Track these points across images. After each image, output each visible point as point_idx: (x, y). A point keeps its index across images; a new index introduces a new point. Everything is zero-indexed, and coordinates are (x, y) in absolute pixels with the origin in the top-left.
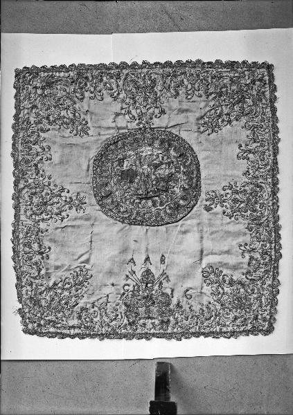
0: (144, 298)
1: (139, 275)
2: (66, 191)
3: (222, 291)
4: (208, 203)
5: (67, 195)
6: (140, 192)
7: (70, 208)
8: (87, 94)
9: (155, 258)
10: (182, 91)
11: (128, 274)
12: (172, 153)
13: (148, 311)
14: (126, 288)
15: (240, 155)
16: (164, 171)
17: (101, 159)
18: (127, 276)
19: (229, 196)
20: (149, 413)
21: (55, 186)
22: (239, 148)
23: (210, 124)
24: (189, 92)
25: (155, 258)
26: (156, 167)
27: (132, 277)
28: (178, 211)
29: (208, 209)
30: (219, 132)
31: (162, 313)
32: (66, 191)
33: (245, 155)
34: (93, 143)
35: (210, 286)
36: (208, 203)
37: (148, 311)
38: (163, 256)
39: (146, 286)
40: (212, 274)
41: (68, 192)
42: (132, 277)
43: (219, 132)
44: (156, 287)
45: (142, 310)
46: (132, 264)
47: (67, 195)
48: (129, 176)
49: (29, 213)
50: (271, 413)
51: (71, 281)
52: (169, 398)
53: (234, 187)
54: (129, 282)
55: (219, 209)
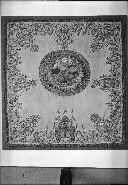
0: (64, 128)
1: (61, 118)
2: (27, 77)
3: (99, 125)
4: (93, 84)
5: (28, 79)
6: (61, 79)
7: (30, 85)
8: (38, 33)
9: (69, 111)
10: (81, 33)
11: (57, 117)
12: (77, 62)
13: (65, 134)
14: (56, 124)
15: (108, 62)
16: (73, 70)
17: (44, 63)
18: (56, 119)
19: (103, 81)
20: (59, 183)
21: (23, 75)
22: (107, 59)
23: (95, 47)
24: (84, 33)
25: (69, 111)
26: (69, 67)
27: (58, 119)
28: (78, 89)
29: (93, 87)
30: (98, 51)
31: (71, 135)
32: (27, 77)
33: (109, 62)
34: (40, 56)
35: (94, 122)
36: (93, 84)
37: (65, 134)
38: (72, 110)
39: (65, 123)
40: (95, 118)
41: (29, 78)
42: (58, 119)
43: (98, 51)
44: (69, 124)
45: (63, 133)
46: (59, 113)
47: (28, 79)
48: (56, 71)
49: (12, 88)
50: (27, 183)
51: (31, 119)
52: (72, 183)
53: (105, 77)
54: (57, 121)
55: (98, 87)
